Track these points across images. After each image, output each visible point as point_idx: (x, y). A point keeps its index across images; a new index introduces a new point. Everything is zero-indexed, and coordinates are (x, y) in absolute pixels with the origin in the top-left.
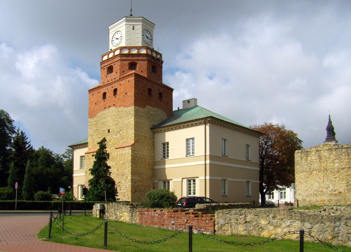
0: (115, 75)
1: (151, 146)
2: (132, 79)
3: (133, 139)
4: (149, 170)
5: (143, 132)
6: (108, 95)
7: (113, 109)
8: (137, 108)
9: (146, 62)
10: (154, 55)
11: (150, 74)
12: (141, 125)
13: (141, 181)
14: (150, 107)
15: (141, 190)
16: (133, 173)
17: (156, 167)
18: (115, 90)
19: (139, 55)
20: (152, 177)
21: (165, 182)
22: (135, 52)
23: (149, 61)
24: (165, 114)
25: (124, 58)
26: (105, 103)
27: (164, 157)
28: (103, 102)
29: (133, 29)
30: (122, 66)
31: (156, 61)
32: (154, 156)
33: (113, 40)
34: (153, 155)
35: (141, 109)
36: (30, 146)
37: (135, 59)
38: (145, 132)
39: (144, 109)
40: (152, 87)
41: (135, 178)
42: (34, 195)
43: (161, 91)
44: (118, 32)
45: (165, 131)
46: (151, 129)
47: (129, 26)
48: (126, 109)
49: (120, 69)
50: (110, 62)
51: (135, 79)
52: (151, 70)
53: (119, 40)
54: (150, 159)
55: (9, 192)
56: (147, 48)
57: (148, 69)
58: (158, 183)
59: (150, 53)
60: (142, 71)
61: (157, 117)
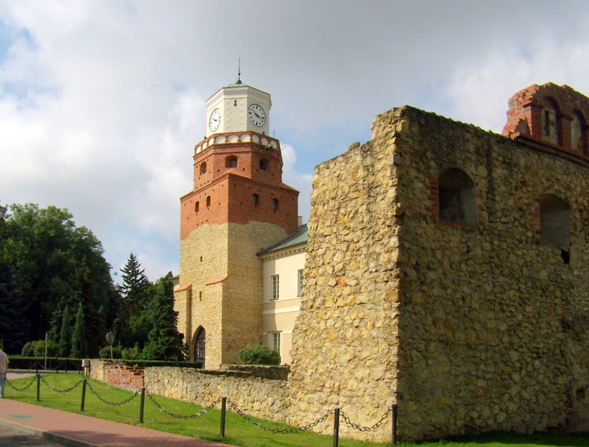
0: (208, 176)
1: (257, 282)
2: (226, 182)
3: (226, 272)
4: (254, 316)
5: (243, 261)
6: (200, 205)
7: (206, 226)
8: (233, 224)
9: (250, 155)
10: (265, 142)
11: (256, 172)
12: (240, 251)
13: (239, 333)
14: (256, 223)
15: (238, 346)
16: (225, 321)
17: (265, 313)
18: (209, 199)
19: (240, 144)
20: (258, 328)
21: (275, 335)
22: (234, 140)
23: (254, 154)
24: (283, 230)
25: (219, 151)
26: (198, 217)
27: (275, 297)
28: (195, 216)
29: (235, 105)
30: (216, 163)
31: (268, 152)
32: (262, 295)
33: (259, 107)
34: (261, 294)
35: (239, 227)
36: (143, 277)
37: (235, 151)
38: (246, 261)
39: (246, 225)
40: (260, 191)
41: (229, 328)
42: (99, 350)
43: (275, 197)
44: (217, 110)
45: (274, 258)
46: (258, 255)
47: (229, 100)
48: (219, 227)
49: (214, 167)
50: (203, 157)
51: (229, 182)
52: (258, 166)
53: (217, 123)
54: (255, 301)
55: (52, 347)
56: (252, 134)
57: (253, 166)
58: (267, 336)
59: (256, 140)
60: (244, 169)
61: (269, 236)
